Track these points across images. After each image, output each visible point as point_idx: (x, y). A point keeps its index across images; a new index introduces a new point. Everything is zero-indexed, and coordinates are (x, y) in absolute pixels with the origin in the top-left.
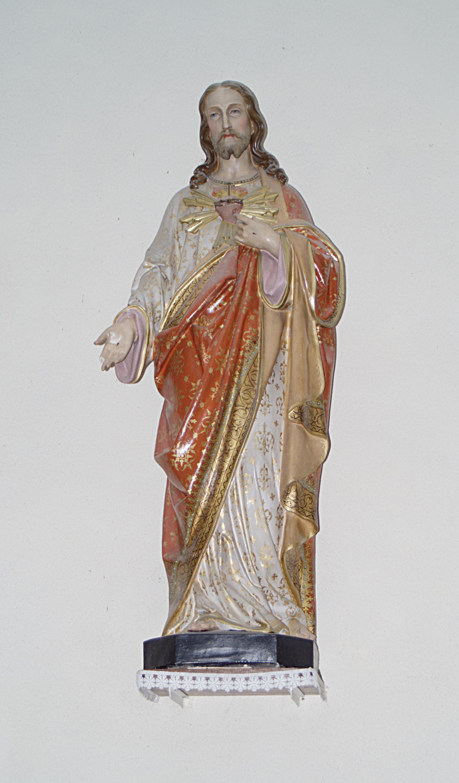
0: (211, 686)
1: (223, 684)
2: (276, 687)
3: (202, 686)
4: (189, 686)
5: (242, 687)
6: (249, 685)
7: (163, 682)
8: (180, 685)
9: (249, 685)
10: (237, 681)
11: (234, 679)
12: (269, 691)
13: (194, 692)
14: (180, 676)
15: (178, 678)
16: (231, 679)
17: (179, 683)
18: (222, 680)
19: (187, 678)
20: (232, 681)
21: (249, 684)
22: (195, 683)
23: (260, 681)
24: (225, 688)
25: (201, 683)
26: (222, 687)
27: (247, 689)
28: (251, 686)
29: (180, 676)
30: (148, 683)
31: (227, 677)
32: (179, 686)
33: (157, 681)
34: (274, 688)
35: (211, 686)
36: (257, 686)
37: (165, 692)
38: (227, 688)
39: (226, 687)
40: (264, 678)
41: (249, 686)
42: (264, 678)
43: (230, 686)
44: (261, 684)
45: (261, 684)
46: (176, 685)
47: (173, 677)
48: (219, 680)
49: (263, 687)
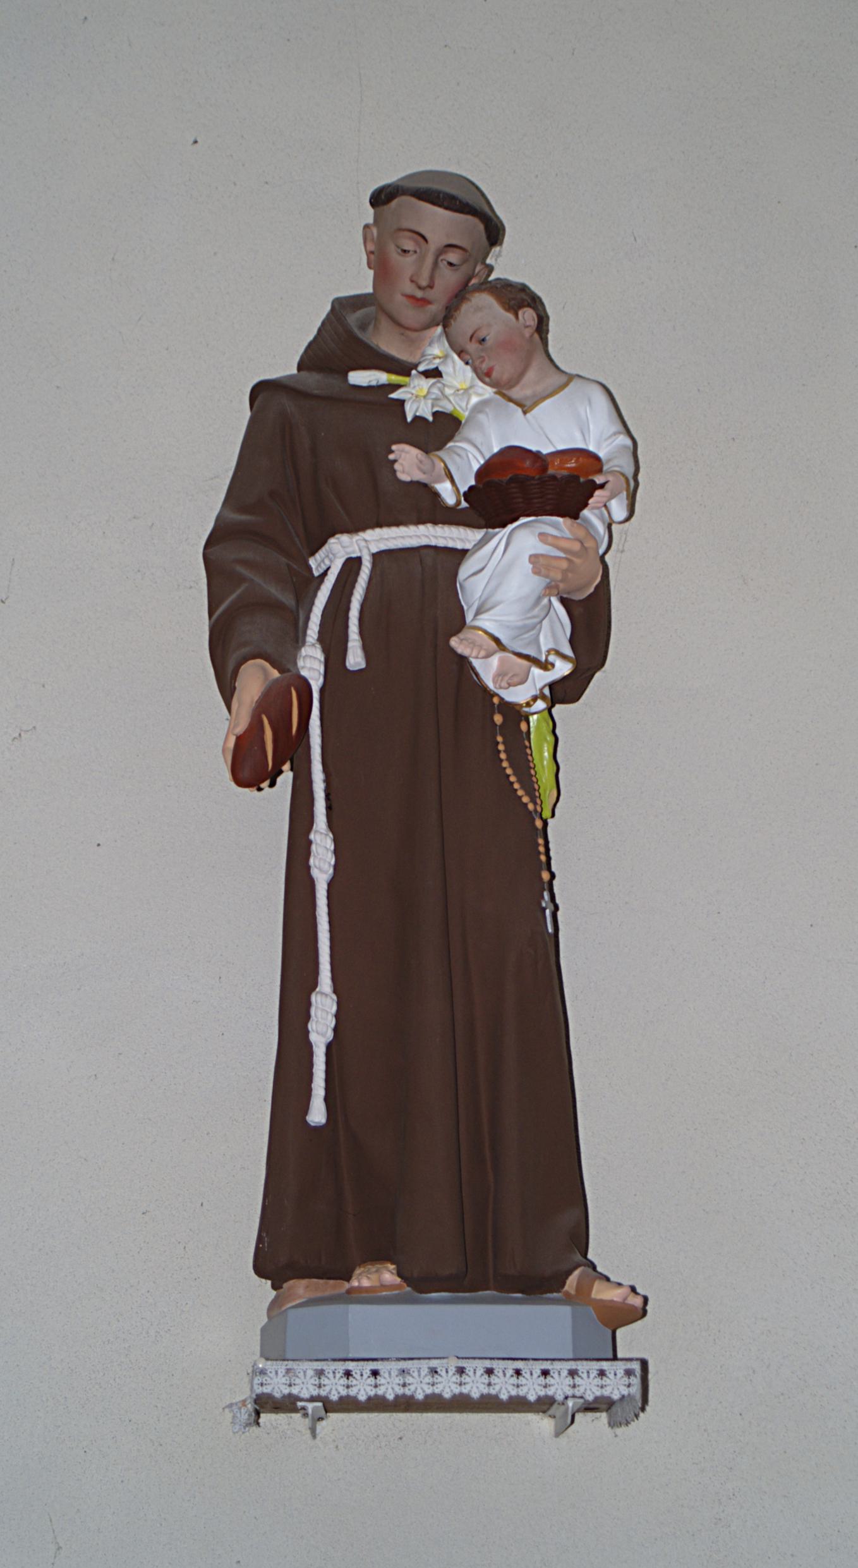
0: (497, 1388)
1: (438, 1381)
2: (437, 1391)
3: (307, 1389)
4: (450, 1387)
5: (477, 1387)
6: (409, 1384)
7: (562, 1384)
8: (430, 1386)
9: (409, 1384)
10: (467, 1375)
11: (545, 1373)
12: (535, 1401)
13: (348, 1405)
14: (513, 1369)
15: (341, 1374)
16: (539, 1372)
17: (596, 1384)
18: (352, 1375)
19: (529, 1373)
20: (542, 1378)
21: (408, 1382)
22: (463, 1381)
23: (518, 1378)
24: (528, 1393)
25: (305, 1383)
26: (350, 1390)
27: (319, 1395)
28: (412, 1388)
29: (513, 1369)
30: (358, 1387)
31: (446, 1365)
32: (429, 1388)
33: (378, 1382)
34: (461, 1394)
35: (412, 1388)
36: (510, 1388)
37: (288, 1405)
38: (475, 1389)
39: (529, 1390)
40: (610, 1373)
41: (323, 1388)
42: (498, 1372)
43: (538, 1388)
44: (546, 1384)
45: (546, 1384)
46: (422, 1388)
47: (270, 1372)
48: (599, 1375)
49: (522, 1392)
